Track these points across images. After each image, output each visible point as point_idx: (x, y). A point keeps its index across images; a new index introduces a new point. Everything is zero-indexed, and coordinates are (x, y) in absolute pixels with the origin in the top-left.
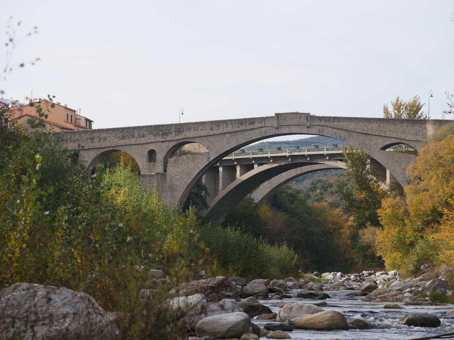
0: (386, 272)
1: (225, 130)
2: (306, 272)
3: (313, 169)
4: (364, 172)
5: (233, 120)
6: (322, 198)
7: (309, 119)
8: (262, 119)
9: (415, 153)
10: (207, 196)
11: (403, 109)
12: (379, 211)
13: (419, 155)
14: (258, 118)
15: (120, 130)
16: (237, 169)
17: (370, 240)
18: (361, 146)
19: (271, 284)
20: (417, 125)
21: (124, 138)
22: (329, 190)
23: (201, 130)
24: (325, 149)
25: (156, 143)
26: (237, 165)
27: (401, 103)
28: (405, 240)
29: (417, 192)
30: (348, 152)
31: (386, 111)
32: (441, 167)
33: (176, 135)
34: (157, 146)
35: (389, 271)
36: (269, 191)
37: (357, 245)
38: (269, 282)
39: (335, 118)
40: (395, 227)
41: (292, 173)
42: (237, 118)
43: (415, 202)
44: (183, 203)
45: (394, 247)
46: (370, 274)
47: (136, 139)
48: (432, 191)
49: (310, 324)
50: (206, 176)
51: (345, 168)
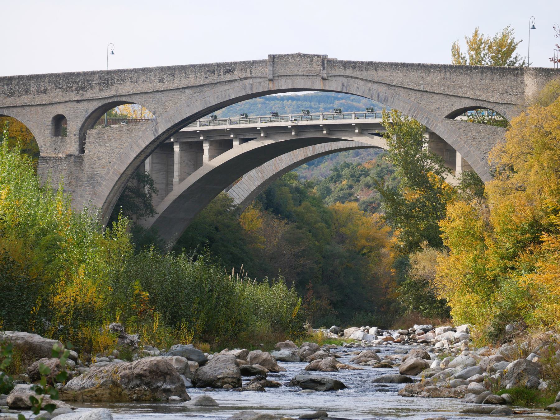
0: (453, 328)
1: (184, 83)
2: (316, 326)
3: (333, 149)
4: (417, 156)
5: (196, 65)
6: (351, 195)
7: (326, 65)
8: (246, 64)
9: (505, 124)
10: (154, 195)
11: (484, 50)
12: (441, 223)
13: (510, 129)
14: (241, 63)
15: (6, 82)
16: (204, 148)
17: (427, 271)
18: (414, 112)
19: (248, 358)
20: (509, 76)
21: (12, 94)
22: (363, 180)
23: (144, 81)
24: (354, 115)
25: (67, 104)
26: (204, 142)
27: (481, 39)
28: (485, 273)
29: (506, 191)
30: (391, 121)
31: (456, 52)
32: (548, 150)
33: (100, 90)
34: (69, 109)
35: (458, 325)
36: (259, 184)
37: (405, 279)
38: (248, 353)
39: (370, 64)
40: (468, 251)
41: (299, 154)
42: (205, 63)
43: (502, 209)
44: (112, 205)
45: (467, 285)
46: (426, 331)
47: (32, 96)
48: (531, 191)
50: (152, 158)
51: (387, 148)
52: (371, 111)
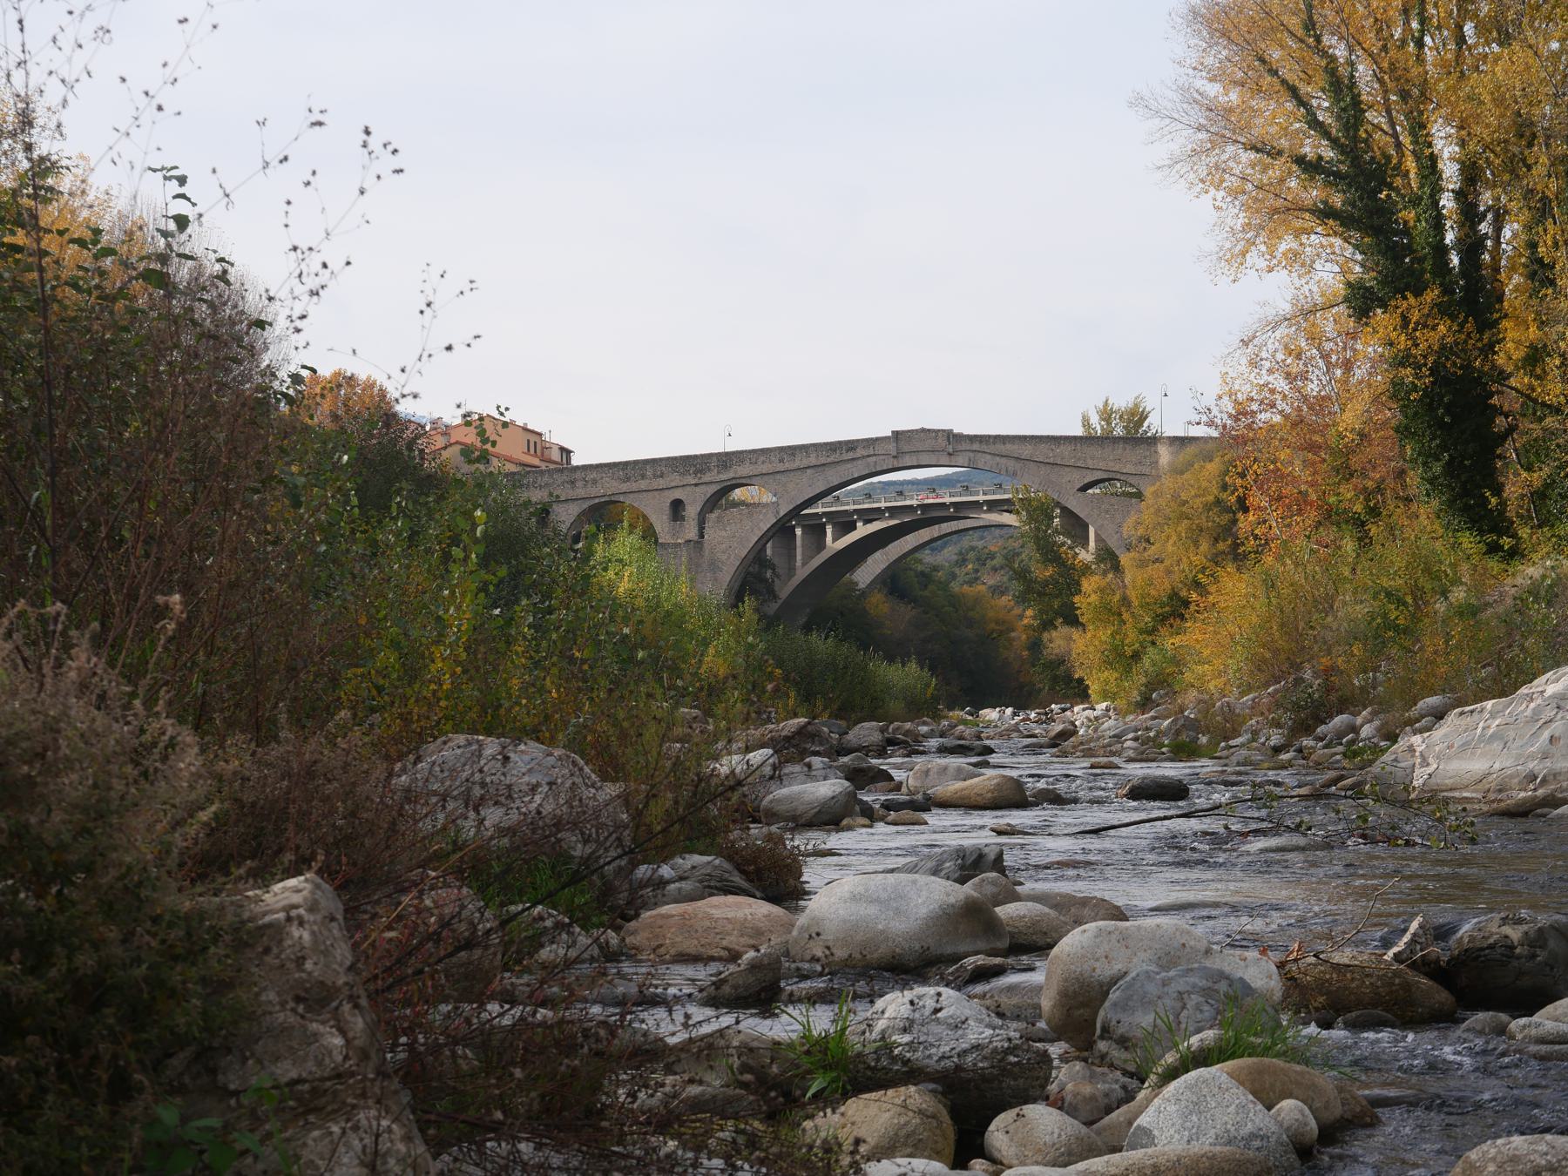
1: (805, 463)
9: (1139, 495)
12: (1076, 599)
21: (628, 479)
22: (990, 563)
29: (1142, 564)
31: (1086, 422)
43: (1139, 582)
46: (1064, 710)
49: (962, 798)
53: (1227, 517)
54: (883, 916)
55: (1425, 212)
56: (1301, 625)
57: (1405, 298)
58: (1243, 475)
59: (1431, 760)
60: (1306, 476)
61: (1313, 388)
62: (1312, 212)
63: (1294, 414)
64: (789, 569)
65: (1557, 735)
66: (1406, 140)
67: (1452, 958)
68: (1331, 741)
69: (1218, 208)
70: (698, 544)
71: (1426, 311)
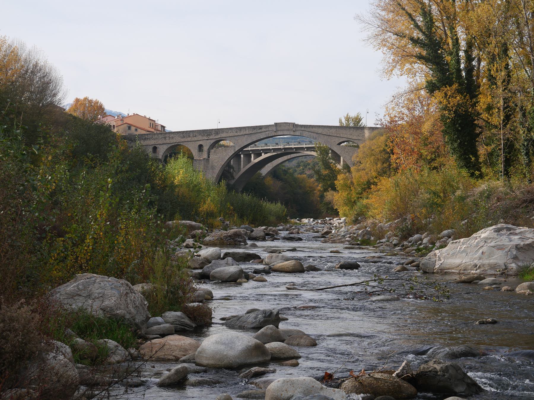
1: (245, 133)
9: (358, 147)
10: (234, 173)
12: (336, 182)
21: (184, 137)
22: (308, 167)
29: (358, 171)
31: (340, 121)
39: (310, 126)
43: (357, 177)
46: (330, 220)
49: (282, 268)
52: (311, 142)
53: (387, 155)
54: (226, 350)
55: (454, 57)
56: (407, 199)
57: (446, 87)
58: (392, 142)
59: (442, 259)
60: (414, 143)
61: (417, 113)
62: (416, 57)
63: (410, 122)
64: (239, 169)
65: (484, 251)
66: (448, 32)
67: (417, 374)
68: (414, 243)
69: (384, 54)
70: (207, 160)
71: (453, 92)
